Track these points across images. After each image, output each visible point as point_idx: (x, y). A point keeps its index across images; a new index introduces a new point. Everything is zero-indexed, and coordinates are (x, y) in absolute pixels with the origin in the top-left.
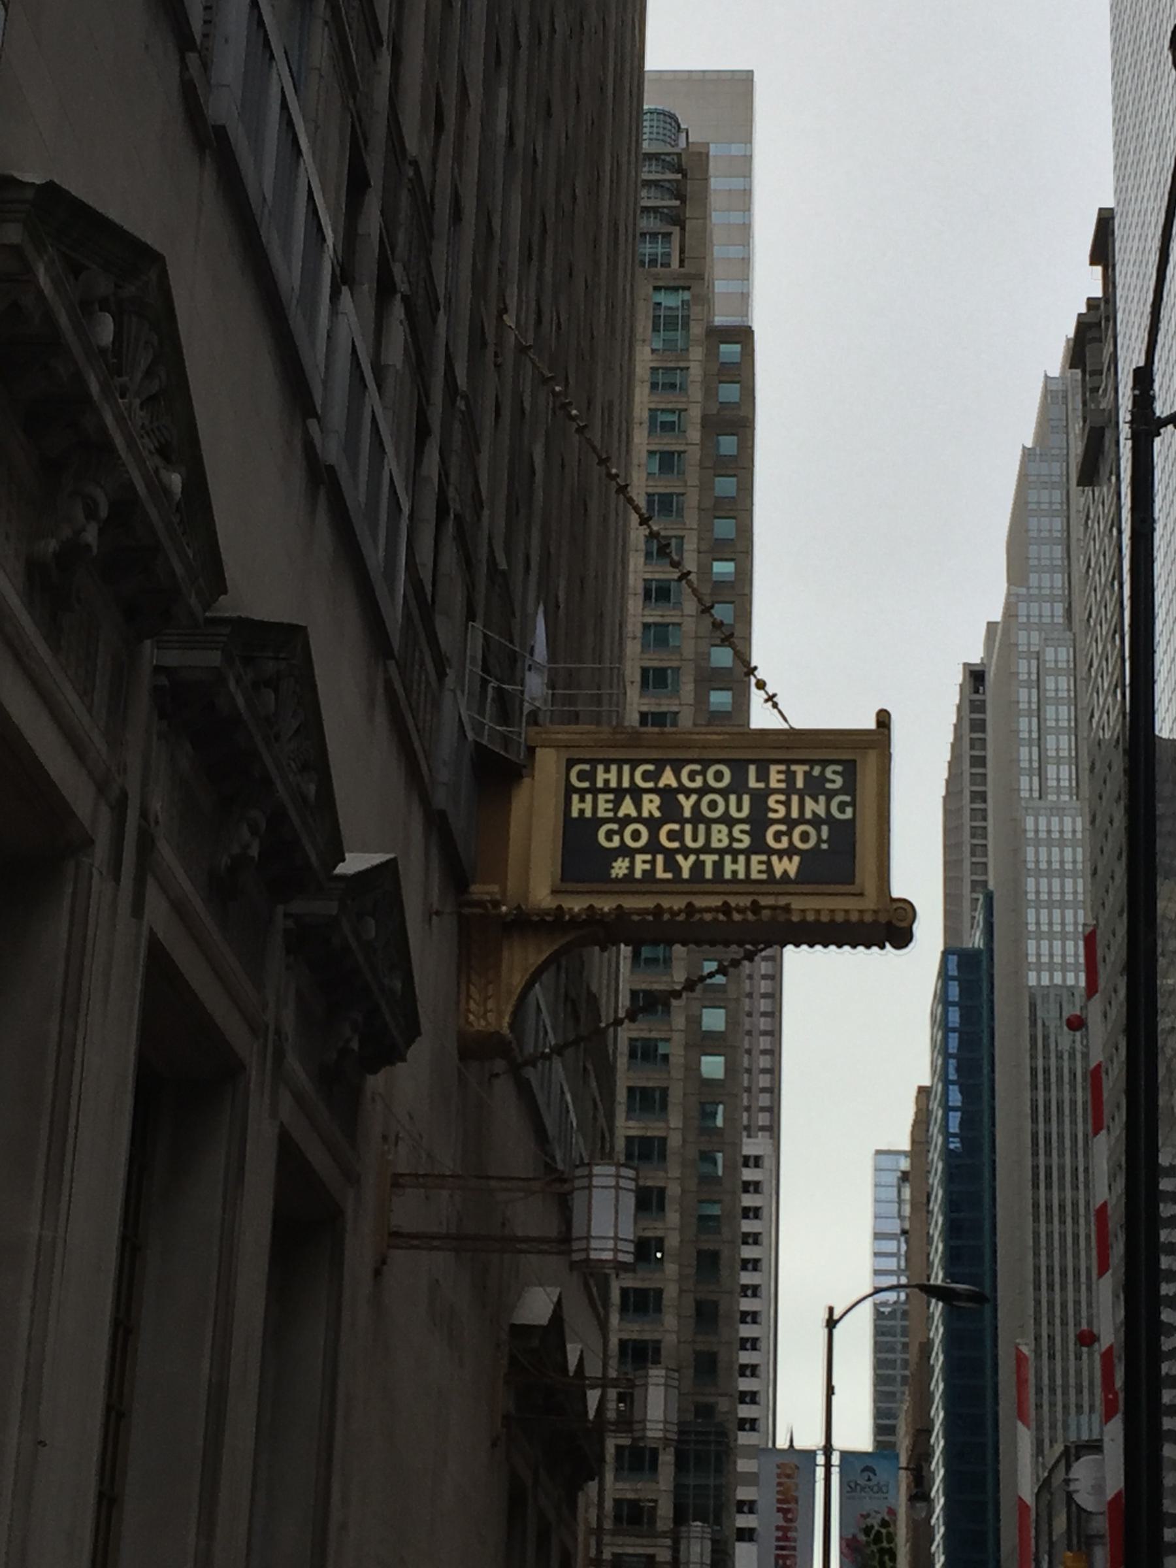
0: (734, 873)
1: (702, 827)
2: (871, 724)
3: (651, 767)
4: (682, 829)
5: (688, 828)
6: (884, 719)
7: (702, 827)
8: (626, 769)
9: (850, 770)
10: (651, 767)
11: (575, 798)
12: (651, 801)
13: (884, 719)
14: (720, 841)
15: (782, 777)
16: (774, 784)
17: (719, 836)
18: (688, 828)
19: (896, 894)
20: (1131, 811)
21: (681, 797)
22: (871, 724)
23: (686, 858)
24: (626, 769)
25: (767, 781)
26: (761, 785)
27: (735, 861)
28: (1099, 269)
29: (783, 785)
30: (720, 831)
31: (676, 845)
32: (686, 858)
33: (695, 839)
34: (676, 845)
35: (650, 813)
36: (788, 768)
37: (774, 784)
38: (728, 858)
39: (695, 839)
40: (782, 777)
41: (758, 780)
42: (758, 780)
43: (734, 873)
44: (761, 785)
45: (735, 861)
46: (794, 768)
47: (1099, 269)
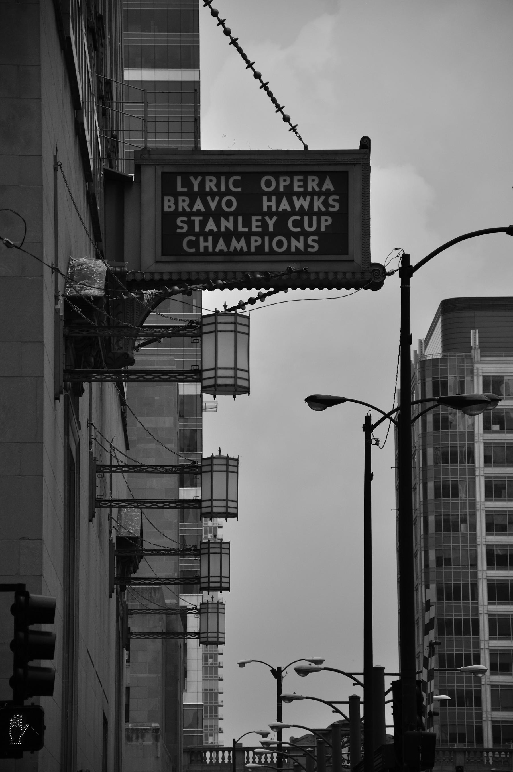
0: (206, 248)
1: (315, 218)
2: (356, 146)
3: (239, 178)
4: (302, 220)
5: (306, 218)
6: (366, 143)
7: (315, 218)
8: (223, 179)
9: (341, 181)
10: (239, 178)
11: (265, 198)
12: (184, 201)
13: (366, 143)
14: (169, 207)
15: (259, 224)
16: (254, 229)
17: (170, 204)
18: (306, 218)
19: (373, 261)
20: (57, 256)
21: (192, 178)
22: (356, 146)
23: (271, 219)
24: (223, 179)
25: (250, 228)
26: (246, 230)
27: (206, 240)
28: (375, 663)
29: (260, 230)
30: (169, 207)
31: (299, 230)
32: (271, 219)
33: (310, 226)
34: (299, 230)
35: (183, 208)
36: (189, 218)
37: (254, 229)
38: (202, 239)
39: (310, 226)
40: (259, 224)
41: (243, 227)
42: (243, 227)
43: (206, 248)
44: (246, 230)
45: (206, 240)
46: (193, 218)
47: (375, 663)
